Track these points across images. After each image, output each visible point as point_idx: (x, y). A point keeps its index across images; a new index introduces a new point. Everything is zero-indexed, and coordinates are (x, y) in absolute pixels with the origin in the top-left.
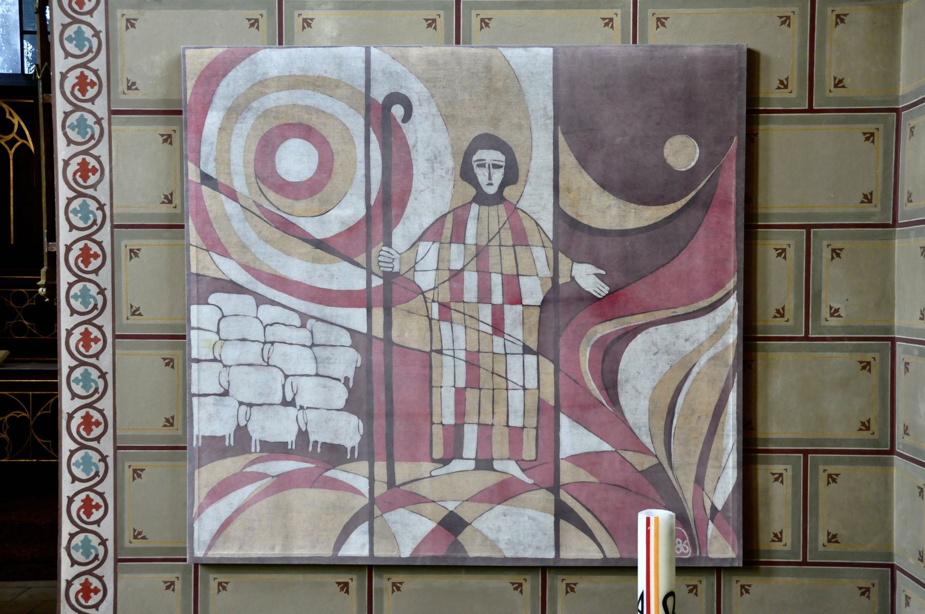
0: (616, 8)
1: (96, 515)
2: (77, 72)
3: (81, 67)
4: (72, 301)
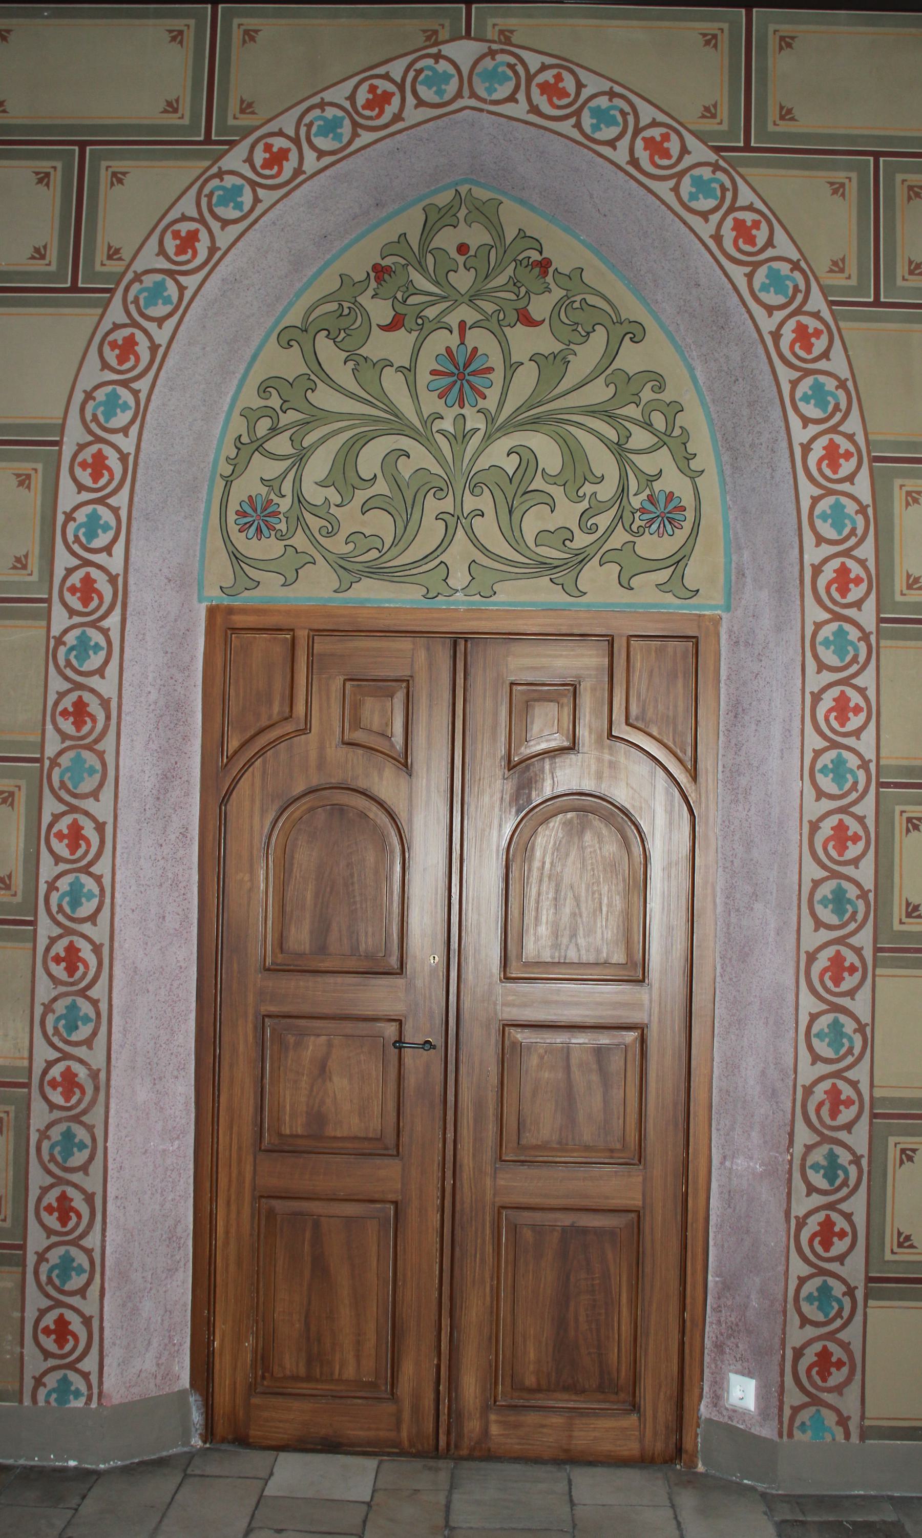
0: (893, 812)
1: (839, 1247)
2: (835, 692)
3: (827, 1209)
4: (815, 1042)
